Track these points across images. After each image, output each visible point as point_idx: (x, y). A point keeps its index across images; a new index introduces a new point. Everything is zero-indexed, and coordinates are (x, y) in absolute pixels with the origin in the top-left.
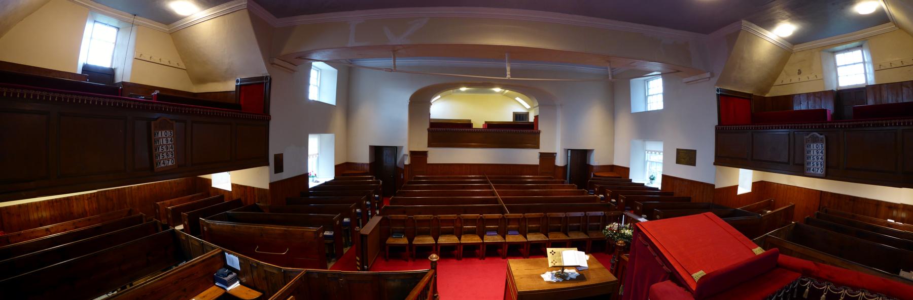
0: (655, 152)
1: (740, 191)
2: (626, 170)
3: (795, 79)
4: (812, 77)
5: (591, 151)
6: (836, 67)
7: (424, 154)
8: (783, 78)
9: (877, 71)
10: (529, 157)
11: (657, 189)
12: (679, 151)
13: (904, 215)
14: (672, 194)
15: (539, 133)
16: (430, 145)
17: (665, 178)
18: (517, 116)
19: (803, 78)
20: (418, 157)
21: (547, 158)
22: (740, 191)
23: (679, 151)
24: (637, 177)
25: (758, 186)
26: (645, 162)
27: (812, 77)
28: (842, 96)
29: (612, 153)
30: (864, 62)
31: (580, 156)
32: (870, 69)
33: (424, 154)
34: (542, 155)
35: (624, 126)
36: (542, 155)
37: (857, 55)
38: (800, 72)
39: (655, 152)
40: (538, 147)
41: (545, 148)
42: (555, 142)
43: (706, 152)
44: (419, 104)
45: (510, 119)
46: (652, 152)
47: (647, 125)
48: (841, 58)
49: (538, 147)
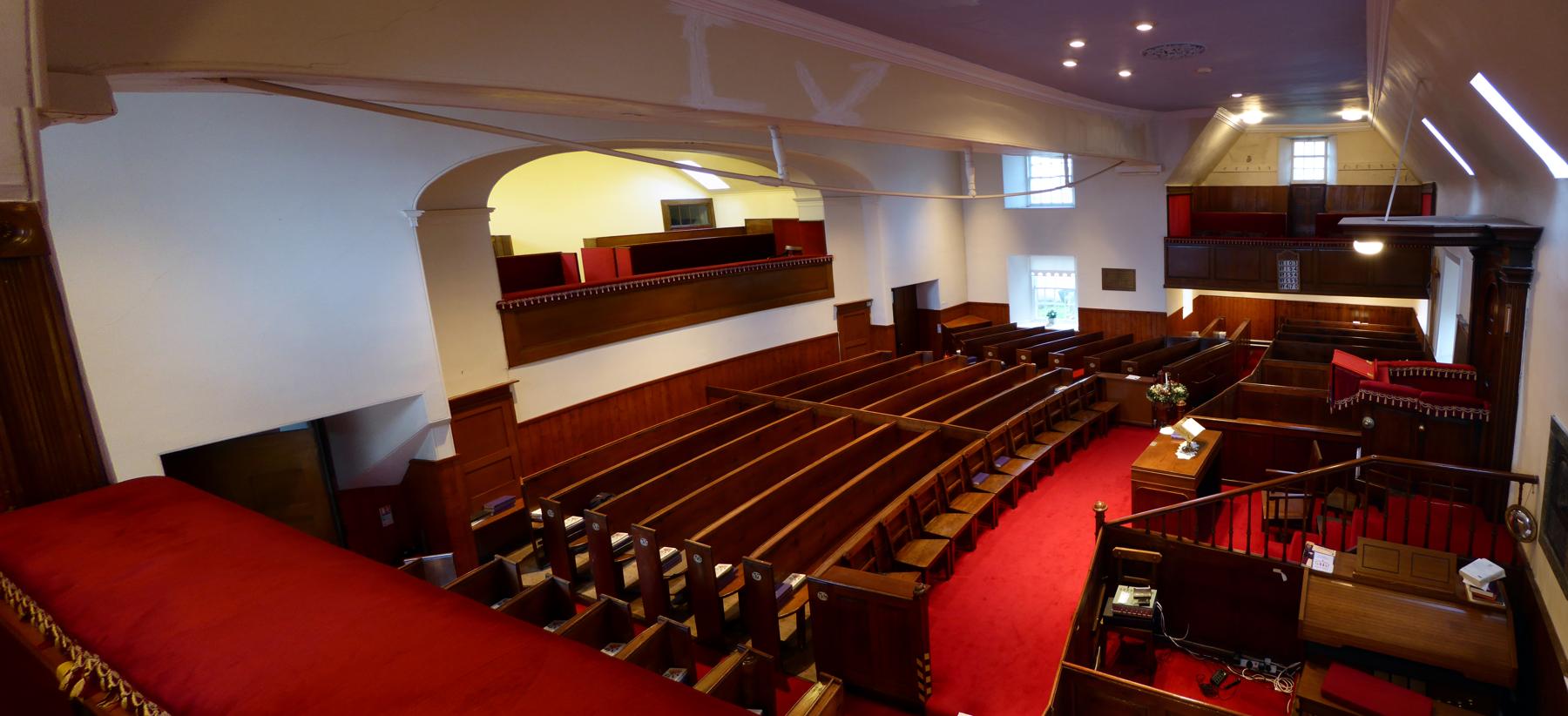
0: (1061, 273)
1: (1185, 314)
2: (1004, 309)
3: (1243, 167)
4: (1264, 167)
5: (933, 283)
6: (1292, 157)
7: (502, 395)
8: (1227, 164)
9: (1340, 171)
10: (813, 321)
11: (1071, 333)
12: (1106, 272)
13: (1363, 315)
14: (1099, 335)
15: (830, 261)
16: (516, 358)
17: (1083, 313)
18: (675, 212)
19: (1253, 167)
20: (480, 412)
21: (853, 314)
22: (1185, 314)
23: (1106, 272)
24: (1024, 318)
25: (1198, 302)
26: (1031, 290)
27: (1264, 167)
28: (1298, 192)
29: (965, 281)
30: (1326, 156)
31: (909, 298)
32: (1331, 165)
33: (502, 395)
34: (842, 311)
35: (988, 231)
36: (842, 311)
37: (1319, 147)
38: (1249, 160)
39: (1061, 273)
40: (831, 295)
41: (845, 292)
42: (866, 275)
43: (1151, 271)
44: (451, 210)
45: (652, 223)
46: (1044, 273)
47: (1039, 232)
48: (1300, 147)
49: (831, 295)
